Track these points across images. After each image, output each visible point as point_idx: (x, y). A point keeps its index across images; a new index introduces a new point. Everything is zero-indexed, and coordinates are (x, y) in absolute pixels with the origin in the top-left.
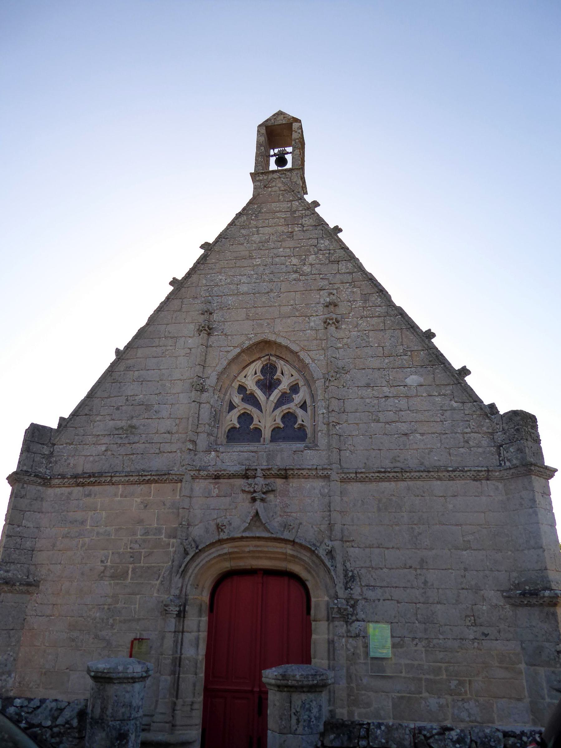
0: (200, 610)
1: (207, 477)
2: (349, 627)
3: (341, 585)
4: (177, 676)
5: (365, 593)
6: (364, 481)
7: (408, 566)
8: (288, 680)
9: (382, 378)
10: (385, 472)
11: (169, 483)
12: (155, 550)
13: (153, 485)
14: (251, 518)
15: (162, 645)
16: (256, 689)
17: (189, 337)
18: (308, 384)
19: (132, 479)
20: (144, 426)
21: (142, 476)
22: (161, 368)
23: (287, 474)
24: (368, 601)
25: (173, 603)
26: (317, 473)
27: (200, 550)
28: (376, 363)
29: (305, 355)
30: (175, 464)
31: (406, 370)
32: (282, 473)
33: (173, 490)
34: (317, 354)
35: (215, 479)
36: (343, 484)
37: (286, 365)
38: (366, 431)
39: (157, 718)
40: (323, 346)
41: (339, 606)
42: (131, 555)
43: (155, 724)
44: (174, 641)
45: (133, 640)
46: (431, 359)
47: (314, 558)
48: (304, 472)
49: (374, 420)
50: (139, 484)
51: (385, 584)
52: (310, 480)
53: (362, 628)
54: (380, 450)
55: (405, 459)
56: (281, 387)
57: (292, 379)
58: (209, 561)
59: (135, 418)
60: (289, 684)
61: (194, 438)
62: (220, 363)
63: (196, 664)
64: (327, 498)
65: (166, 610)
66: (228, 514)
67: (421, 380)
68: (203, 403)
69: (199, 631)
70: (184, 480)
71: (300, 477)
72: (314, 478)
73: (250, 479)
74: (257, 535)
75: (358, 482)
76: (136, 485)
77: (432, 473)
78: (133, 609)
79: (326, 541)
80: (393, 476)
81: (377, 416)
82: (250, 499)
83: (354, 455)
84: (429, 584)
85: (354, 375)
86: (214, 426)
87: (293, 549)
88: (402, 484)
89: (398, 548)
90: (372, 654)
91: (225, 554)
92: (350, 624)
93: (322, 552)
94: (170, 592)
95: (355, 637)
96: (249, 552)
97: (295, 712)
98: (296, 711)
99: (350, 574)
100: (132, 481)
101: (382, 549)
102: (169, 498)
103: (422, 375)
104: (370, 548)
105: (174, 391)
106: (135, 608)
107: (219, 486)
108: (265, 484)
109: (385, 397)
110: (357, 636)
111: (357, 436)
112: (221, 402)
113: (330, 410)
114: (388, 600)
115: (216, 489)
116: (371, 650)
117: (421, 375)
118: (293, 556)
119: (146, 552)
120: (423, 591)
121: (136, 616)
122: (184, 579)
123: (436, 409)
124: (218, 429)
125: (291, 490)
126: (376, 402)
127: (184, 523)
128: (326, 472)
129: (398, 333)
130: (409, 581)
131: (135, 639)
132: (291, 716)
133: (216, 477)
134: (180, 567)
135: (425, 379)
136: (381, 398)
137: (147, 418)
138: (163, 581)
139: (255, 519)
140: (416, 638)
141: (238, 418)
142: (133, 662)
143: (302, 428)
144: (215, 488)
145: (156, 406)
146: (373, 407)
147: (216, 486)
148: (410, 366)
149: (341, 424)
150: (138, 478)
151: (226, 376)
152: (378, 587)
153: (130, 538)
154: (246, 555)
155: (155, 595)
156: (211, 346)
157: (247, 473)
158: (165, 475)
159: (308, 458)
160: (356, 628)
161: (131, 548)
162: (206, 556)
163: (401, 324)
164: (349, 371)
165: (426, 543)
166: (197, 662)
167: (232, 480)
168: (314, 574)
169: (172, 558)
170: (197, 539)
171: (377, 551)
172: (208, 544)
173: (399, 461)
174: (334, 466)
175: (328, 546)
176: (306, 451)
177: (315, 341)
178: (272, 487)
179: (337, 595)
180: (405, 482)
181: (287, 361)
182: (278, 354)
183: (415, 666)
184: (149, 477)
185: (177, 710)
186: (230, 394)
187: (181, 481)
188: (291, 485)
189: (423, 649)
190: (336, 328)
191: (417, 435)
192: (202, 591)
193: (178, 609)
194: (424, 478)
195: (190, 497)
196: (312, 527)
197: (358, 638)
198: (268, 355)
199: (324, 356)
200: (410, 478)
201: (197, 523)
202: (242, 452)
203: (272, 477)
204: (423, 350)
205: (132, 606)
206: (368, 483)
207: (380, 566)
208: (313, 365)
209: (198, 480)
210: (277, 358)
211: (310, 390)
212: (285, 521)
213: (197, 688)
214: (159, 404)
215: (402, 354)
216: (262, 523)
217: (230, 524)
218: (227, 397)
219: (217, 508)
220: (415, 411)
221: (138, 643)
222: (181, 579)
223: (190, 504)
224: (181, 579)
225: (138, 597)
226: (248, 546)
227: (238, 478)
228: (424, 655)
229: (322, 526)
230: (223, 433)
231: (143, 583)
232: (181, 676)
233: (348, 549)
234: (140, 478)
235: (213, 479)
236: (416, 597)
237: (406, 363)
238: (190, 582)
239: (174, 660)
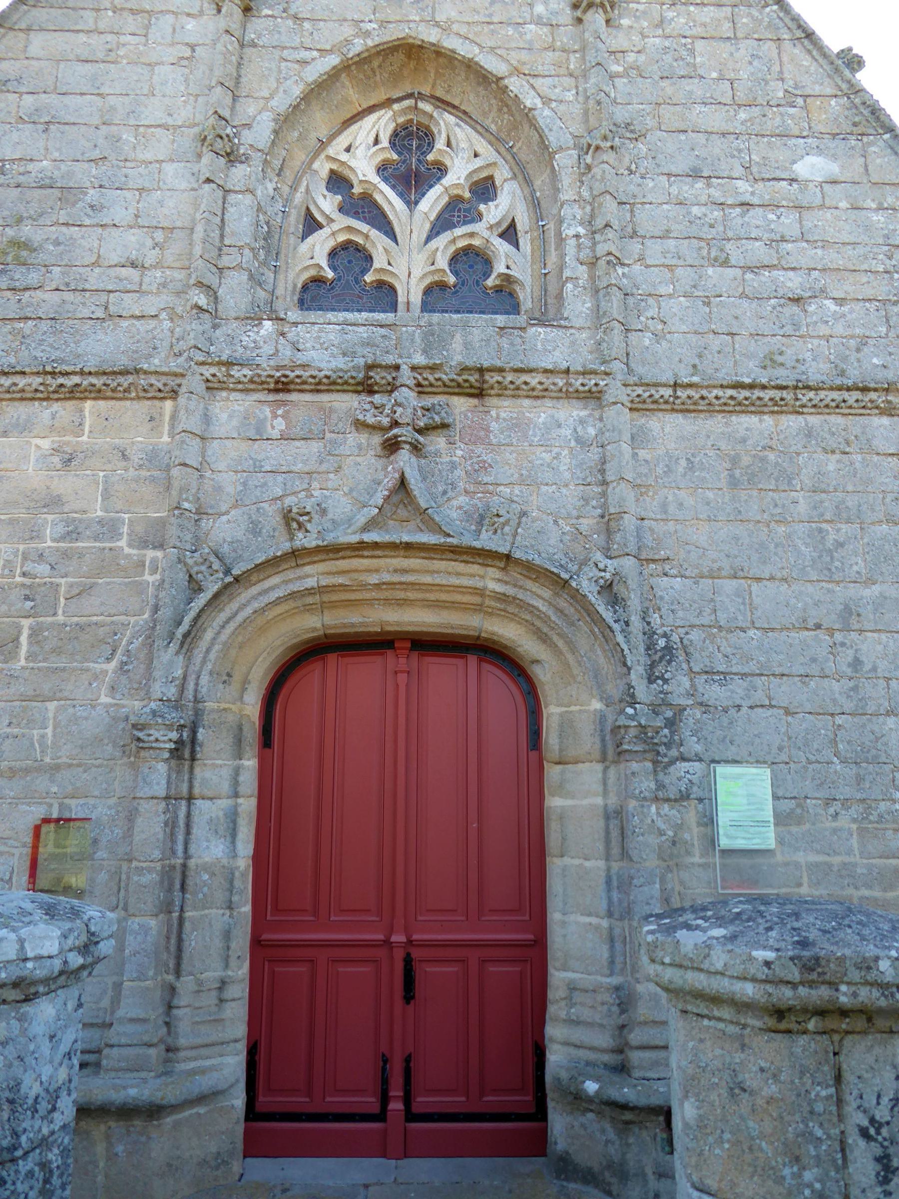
0: (239, 742)
1: (252, 386)
2: (661, 776)
3: (640, 669)
4: (176, 915)
5: (701, 690)
6: (694, 411)
7: (810, 624)
8: (833, 985)
9: (733, 157)
10: (751, 387)
11: (138, 398)
12: (100, 581)
13: (88, 404)
14: (386, 493)
15: (129, 833)
16: (398, 938)
17: (188, 15)
18: (522, 174)
19: (22, 382)
20: (57, 243)
21: (53, 374)
22: (105, 90)
23: (484, 382)
24: (712, 709)
25: (160, 721)
26: (568, 384)
27: (237, 579)
28: (716, 119)
29: (522, 86)
30: (155, 348)
31: (794, 141)
32: (472, 379)
33: (151, 419)
34: (555, 87)
35: (277, 391)
36: (636, 415)
37: (459, 126)
38: (694, 287)
39: (120, 1033)
40: (572, 67)
41: (643, 722)
42: (28, 592)
43: (115, 1049)
44: (166, 824)
45: (39, 822)
46: (857, 119)
48: (534, 380)
49: (716, 260)
50: (47, 399)
51: (752, 667)
52: (548, 403)
53: (695, 779)
54: (733, 334)
55: (798, 361)
56: (447, 181)
57: (478, 163)
58: (263, 610)
59: (25, 222)
60: (843, 999)
61: (213, 280)
62: (281, 90)
63: (231, 882)
64: (595, 449)
65: (139, 740)
66: (315, 485)
67: (833, 168)
68: (236, 192)
69: (236, 795)
70: (183, 389)
71: (520, 393)
72: (558, 398)
73: (376, 396)
74: (406, 538)
75: (677, 411)
76: (36, 403)
77: (873, 395)
78: (36, 738)
79: (598, 556)
80: (771, 399)
81: (722, 250)
82: (379, 449)
83: (664, 343)
84: (867, 667)
85: (659, 144)
86: (264, 263)
87: (505, 578)
88: (791, 423)
89: (784, 580)
90: (724, 842)
91: (310, 591)
92: (665, 768)
93: (587, 587)
94: (148, 692)
95: (676, 800)
96: (378, 586)
97: (865, 1123)
98: (872, 1120)
99: (662, 643)
100: (23, 391)
101: (743, 581)
102: (139, 439)
103: (834, 158)
104: (713, 578)
105: (149, 156)
106: (43, 736)
107: (287, 412)
108: (422, 408)
109: (742, 204)
110: (684, 797)
111: (670, 296)
112: (284, 206)
113: (599, 223)
114: (762, 706)
115: (280, 419)
116: (721, 832)
117: (833, 155)
118: (503, 598)
119: (71, 586)
120: (851, 684)
121: (47, 760)
122: (189, 659)
123: (873, 241)
124: (275, 272)
125: (494, 426)
126: (717, 214)
127: (186, 505)
128: (593, 382)
129: (769, 49)
130: (814, 660)
131: (46, 821)
132: (843, 1143)
133: (280, 386)
134: (179, 624)
135: (842, 167)
136: (732, 206)
137: (66, 224)
138: (126, 663)
139: (395, 499)
140: (835, 799)
141: (330, 255)
142: (23, 912)
143: (507, 283)
144: (275, 416)
145: (91, 192)
146: (712, 226)
147: (280, 412)
148: (805, 134)
149: (628, 265)
150: (40, 380)
151: (296, 134)
152: (735, 674)
153: (21, 547)
154: (368, 595)
155: (104, 699)
156: (254, 45)
157: (371, 378)
158: (125, 373)
159: (539, 346)
160: (679, 779)
161: (24, 574)
162: (254, 598)
163: (778, 28)
164: (645, 136)
165: (855, 568)
166: (233, 874)
167: (324, 397)
168: (560, 643)
169: (152, 601)
170: (226, 549)
171: (730, 585)
172: (260, 561)
173: (782, 365)
174: (617, 366)
175: (604, 571)
176: (534, 329)
177: (550, 54)
178: (443, 414)
179: (633, 696)
180: (800, 418)
181: (465, 113)
182: (439, 93)
183: (835, 869)
184: (76, 379)
185: (179, 1007)
186: (307, 191)
187: (174, 394)
188: (493, 413)
189: (854, 826)
190: (608, 21)
191: (827, 302)
192: (244, 690)
193: (174, 735)
194: (850, 407)
195: (203, 438)
196: (555, 522)
197: (685, 804)
198: (410, 96)
199: (574, 92)
200: (815, 406)
201: (224, 509)
202: (351, 325)
203: (440, 390)
204: (836, 96)
205: (35, 732)
206: (702, 416)
207: (740, 624)
208: (547, 112)
209: (224, 394)
210: (437, 107)
211: (527, 191)
212: (480, 505)
213: (233, 945)
214: (101, 186)
215: (783, 102)
216: (417, 507)
217: (324, 512)
218: (298, 195)
219: (284, 469)
220: (819, 244)
221: (56, 831)
222: (181, 657)
223: (203, 457)
224: (181, 657)
225: (52, 706)
226: (377, 571)
227: (344, 391)
228: (854, 842)
229: (581, 520)
230: (290, 288)
231: (64, 670)
232: (188, 914)
233: (653, 581)
234: (49, 380)
235: (270, 391)
236: (834, 700)
237: (792, 126)
238: (209, 666)
239: (167, 873)
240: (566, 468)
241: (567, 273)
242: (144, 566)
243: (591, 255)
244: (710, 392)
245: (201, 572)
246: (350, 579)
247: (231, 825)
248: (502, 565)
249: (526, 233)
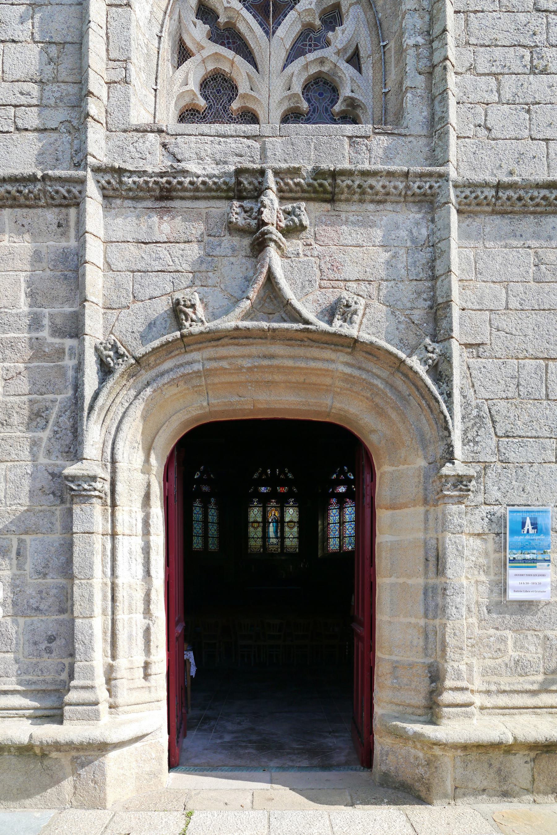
6: (511, 212)
26: (408, 187)
33: (59, 225)
35: (161, 198)
47: (399, 381)
52: (389, 206)
82: (249, 250)
91: (197, 373)
141: (201, 85)
203: (299, 195)
209: (119, 202)
240: (402, 265)
241: (408, 83)
242: (64, 352)
243: (428, 64)
244: (527, 193)
245: (110, 356)
246: (230, 364)
247: (146, 555)
248: (349, 350)
249: (369, 56)
